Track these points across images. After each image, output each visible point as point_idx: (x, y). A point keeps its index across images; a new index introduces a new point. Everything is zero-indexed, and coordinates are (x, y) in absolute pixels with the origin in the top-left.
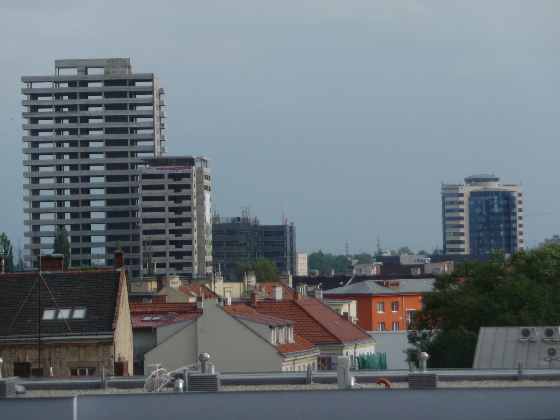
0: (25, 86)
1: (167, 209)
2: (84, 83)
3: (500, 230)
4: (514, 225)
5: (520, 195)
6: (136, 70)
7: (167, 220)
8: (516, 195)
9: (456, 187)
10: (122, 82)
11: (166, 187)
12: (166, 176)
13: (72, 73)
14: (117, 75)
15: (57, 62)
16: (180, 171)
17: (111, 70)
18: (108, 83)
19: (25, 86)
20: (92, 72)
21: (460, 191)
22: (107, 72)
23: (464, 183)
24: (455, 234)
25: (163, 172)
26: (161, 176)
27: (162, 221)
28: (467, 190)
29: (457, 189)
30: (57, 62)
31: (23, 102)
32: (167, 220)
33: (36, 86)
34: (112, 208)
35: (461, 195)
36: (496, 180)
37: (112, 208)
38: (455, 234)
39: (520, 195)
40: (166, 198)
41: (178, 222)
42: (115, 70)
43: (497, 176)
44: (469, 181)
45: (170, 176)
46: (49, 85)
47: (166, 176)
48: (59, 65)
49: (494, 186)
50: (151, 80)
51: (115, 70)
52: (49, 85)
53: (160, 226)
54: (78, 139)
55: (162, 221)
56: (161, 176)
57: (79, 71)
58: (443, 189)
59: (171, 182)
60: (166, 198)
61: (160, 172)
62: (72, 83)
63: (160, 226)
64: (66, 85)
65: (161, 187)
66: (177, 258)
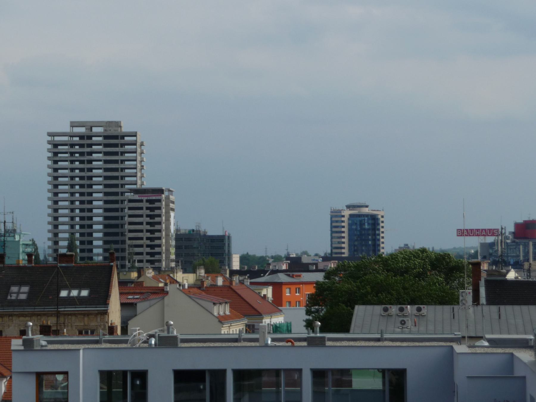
0: (49, 138)
1: (145, 223)
2: (90, 137)
3: (369, 240)
4: (378, 237)
5: (382, 217)
6: (126, 128)
7: (145, 231)
8: (379, 217)
9: (340, 211)
10: (116, 137)
11: (144, 208)
12: (144, 201)
13: (82, 130)
14: (112, 132)
15: (71, 122)
16: (154, 198)
17: (108, 129)
18: (106, 137)
19: (49, 138)
20: (95, 130)
21: (343, 214)
22: (105, 130)
23: (345, 208)
24: (339, 243)
25: (143, 198)
26: (141, 201)
27: (141, 231)
28: (347, 213)
29: (341, 212)
30: (71, 122)
31: (48, 149)
32: (145, 231)
33: (56, 138)
34: (107, 222)
35: (343, 216)
36: (367, 206)
37: (107, 222)
38: (339, 243)
39: (382, 217)
40: (145, 216)
41: (152, 232)
42: (110, 129)
43: (367, 204)
44: (348, 207)
45: (147, 201)
46: (66, 138)
47: (144, 201)
48: (73, 125)
49: (365, 211)
50: (135, 136)
51: (110, 129)
52: (66, 138)
53: (140, 235)
54: (86, 175)
55: (141, 231)
56: (141, 201)
57: (86, 129)
58: (331, 212)
59: (148, 205)
60: (145, 216)
61: (140, 198)
62: (82, 137)
63: (140, 235)
64: (77, 139)
65: (141, 208)
66: (151, 257)
